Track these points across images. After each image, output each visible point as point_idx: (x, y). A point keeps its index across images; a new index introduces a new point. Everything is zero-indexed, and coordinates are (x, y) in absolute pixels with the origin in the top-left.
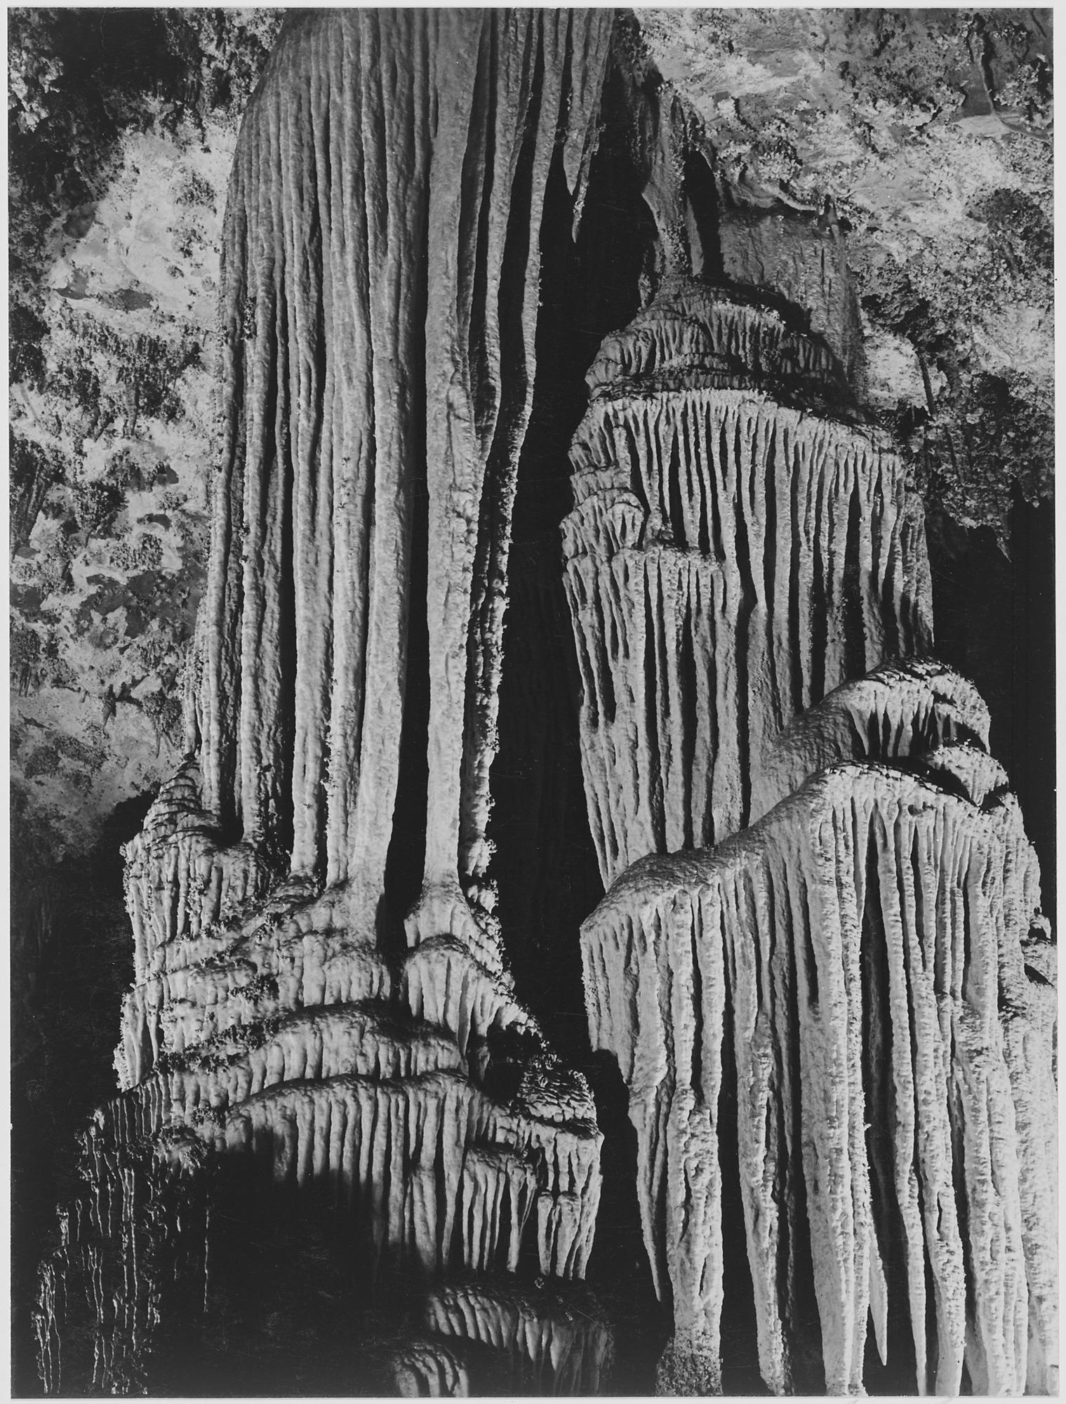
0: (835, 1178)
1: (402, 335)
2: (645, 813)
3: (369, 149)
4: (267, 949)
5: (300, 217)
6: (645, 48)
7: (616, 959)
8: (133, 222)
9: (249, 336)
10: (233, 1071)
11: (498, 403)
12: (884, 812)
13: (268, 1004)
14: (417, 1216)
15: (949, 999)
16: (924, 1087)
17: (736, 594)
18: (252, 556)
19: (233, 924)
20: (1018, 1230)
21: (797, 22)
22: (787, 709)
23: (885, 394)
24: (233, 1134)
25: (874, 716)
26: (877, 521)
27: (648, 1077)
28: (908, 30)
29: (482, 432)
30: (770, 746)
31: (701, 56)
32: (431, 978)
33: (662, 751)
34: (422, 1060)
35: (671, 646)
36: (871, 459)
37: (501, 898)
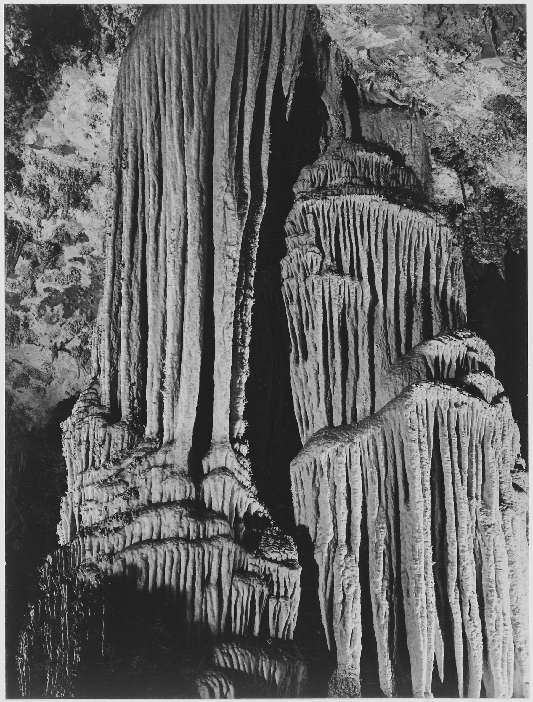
0: (418, 589)
1: (201, 168)
2: (323, 406)
3: (185, 75)
4: (133, 475)
5: (150, 108)
6: (323, 24)
7: (308, 479)
8: (66, 111)
9: (125, 168)
10: (117, 536)
12: (442, 406)
13: (134, 502)
14: (208, 608)
15: (474, 500)
16: (462, 544)
18: (126, 278)
19: (117, 462)
22: (394, 354)
23: (443, 197)
24: (117, 567)
25: (437, 358)
26: (439, 261)
27: (324, 538)
29: (241, 216)
30: (385, 373)
31: (351, 28)
32: (216, 489)
33: (331, 375)
34: (211, 529)
35: (336, 323)
36: (436, 229)
37: (251, 449)
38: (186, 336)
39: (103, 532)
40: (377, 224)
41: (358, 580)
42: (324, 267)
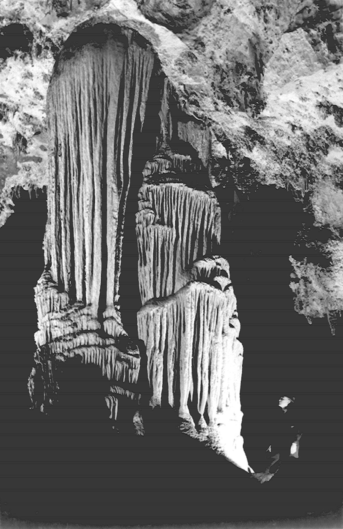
0: (185, 367)
1: (101, 168)
2: (152, 289)
3: (92, 111)
4: (74, 317)
7: (144, 321)
8: (8, 81)
9: (60, 156)
11: (122, 186)
12: (202, 292)
16: (205, 349)
17: (175, 236)
19: (65, 310)
20: (220, 378)
21: (201, 68)
23: (219, 154)
24: (72, 355)
25: (203, 268)
27: (150, 346)
28: (229, 78)
29: (119, 194)
30: (180, 274)
31: (176, 72)
32: (109, 325)
34: (108, 342)
35: (160, 250)
36: (209, 200)
38: (95, 256)
39: (64, 340)
40: (181, 198)
41: (162, 363)
42: (156, 221)
